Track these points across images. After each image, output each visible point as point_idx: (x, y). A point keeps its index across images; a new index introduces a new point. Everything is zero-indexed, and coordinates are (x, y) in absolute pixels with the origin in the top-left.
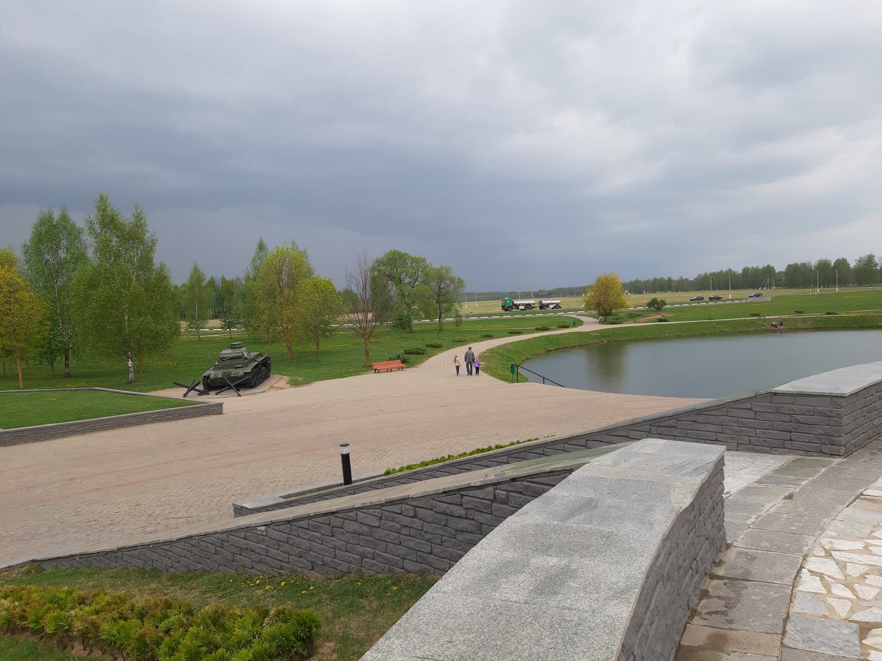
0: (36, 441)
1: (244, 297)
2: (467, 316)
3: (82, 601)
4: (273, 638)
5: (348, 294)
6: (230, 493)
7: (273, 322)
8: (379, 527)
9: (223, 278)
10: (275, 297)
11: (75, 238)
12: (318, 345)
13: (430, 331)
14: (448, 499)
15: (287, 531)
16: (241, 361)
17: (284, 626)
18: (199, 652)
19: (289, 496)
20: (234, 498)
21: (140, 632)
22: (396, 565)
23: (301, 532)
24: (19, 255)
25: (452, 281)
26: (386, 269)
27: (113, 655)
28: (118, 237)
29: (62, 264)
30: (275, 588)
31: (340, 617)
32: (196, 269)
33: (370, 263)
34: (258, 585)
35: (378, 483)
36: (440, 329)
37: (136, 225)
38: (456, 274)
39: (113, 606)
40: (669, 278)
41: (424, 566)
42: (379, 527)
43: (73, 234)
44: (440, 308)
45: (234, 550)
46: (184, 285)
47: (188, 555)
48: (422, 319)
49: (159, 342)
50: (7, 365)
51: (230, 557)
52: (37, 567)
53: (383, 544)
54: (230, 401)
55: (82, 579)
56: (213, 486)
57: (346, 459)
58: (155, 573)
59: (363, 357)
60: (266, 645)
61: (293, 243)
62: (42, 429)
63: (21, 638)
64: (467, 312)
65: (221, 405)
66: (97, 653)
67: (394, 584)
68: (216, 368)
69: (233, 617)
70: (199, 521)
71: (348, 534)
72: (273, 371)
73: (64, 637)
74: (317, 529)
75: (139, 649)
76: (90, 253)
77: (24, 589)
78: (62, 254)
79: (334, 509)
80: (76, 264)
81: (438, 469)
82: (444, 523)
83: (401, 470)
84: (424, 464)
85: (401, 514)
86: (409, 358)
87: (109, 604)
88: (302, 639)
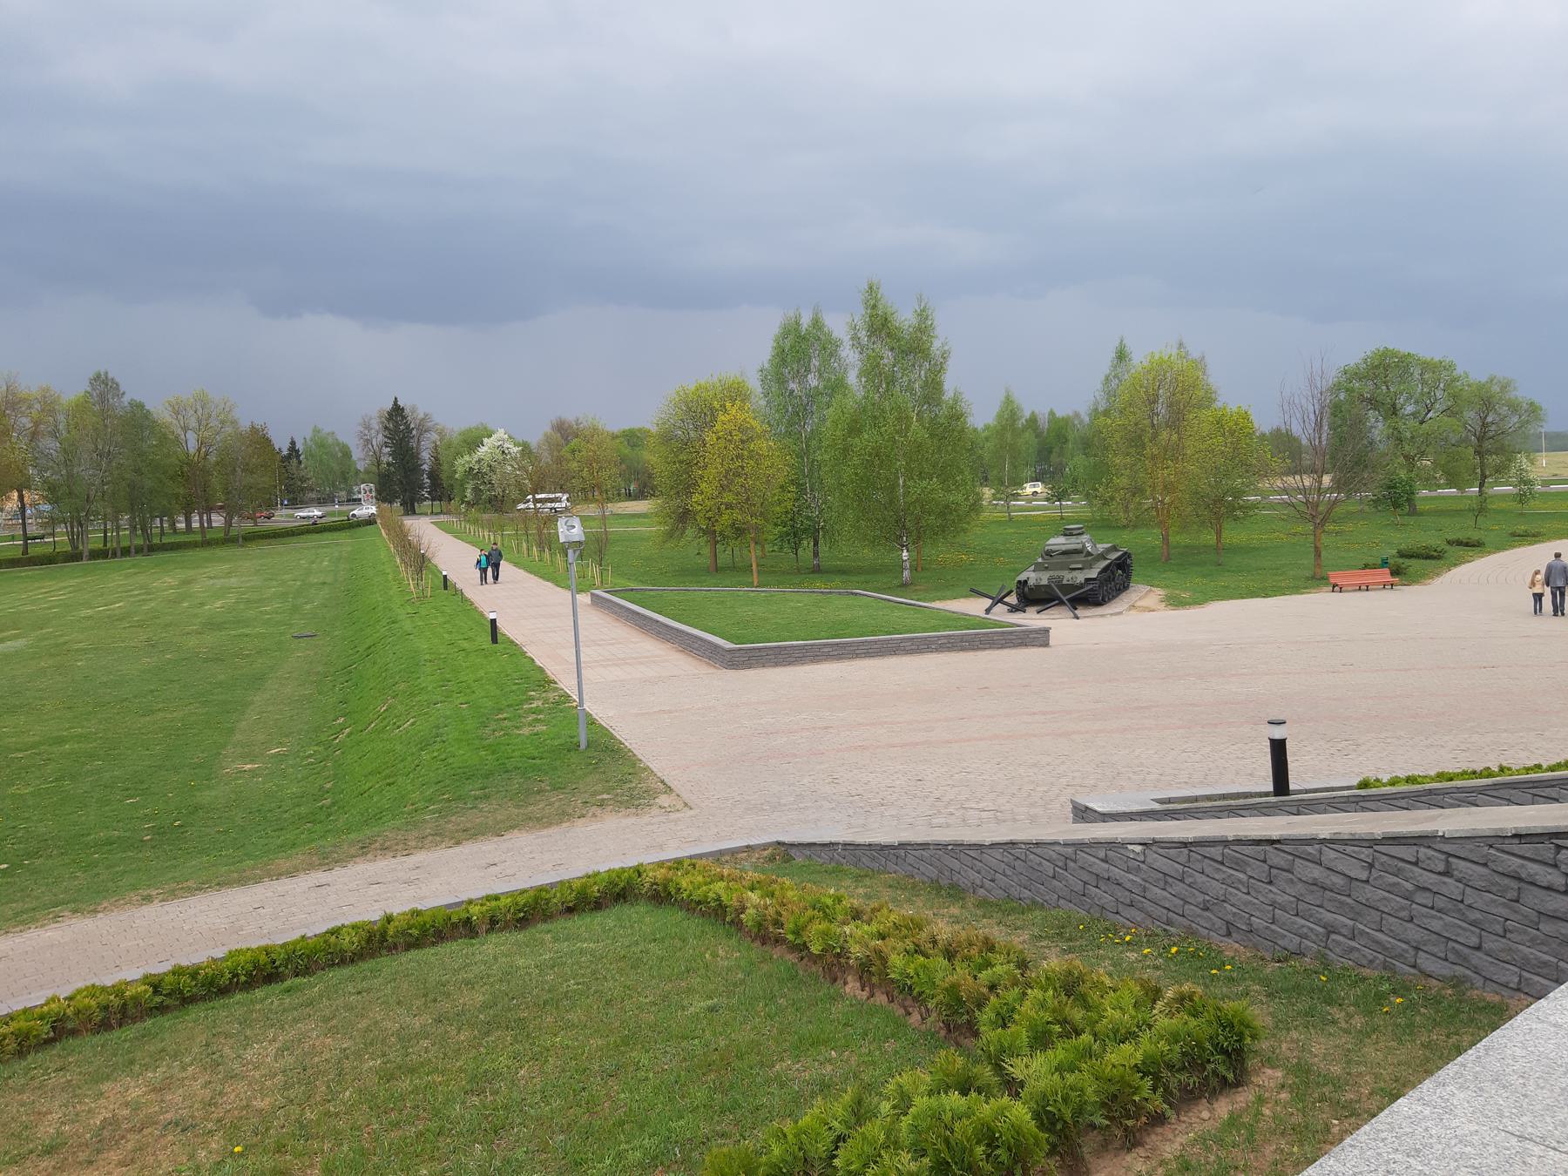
0: (776, 665)
1: (1086, 445)
2: (1546, 483)
3: (856, 915)
4: (1174, 1038)
5: (1283, 442)
6: (1064, 781)
7: (1137, 491)
8: (1367, 881)
9: (1052, 413)
10: (1144, 446)
11: (831, 355)
12: (1219, 534)
13: (1459, 512)
14: (1526, 849)
15: (1182, 859)
16: (1081, 558)
17: (1193, 1022)
18: (1050, 1032)
19: (1169, 801)
20: (1070, 790)
21: (950, 979)
22: (1399, 957)
23: (1208, 866)
24: (754, 385)
25: (1514, 408)
26: (1367, 389)
27: (905, 1008)
28: (892, 349)
29: (813, 395)
30: (1160, 955)
31: (1288, 1030)
32: (1008, 401)
33: (1332, 376)
34: (1128, 943)
35: (1347, 800)
36: (1481, 509)
37: (919, 329)
38: (1523, 392)
39: (905, 931)
40: (104, 386)
41: (1459, 970)
42: (1367, 881)
43: (829, 348)
44: (1482, 465)
45: (1086, 877)
46: (987, 428)
47: (1008, 872)
48: (1439, 487)
49: (947, 521)
50: (736, 549)
51: (1079, 887)
52: (784, 852)
53: (1376, 915)
54: (1059, 623)
55: (848, 882)
56: (1035, 765)
57: (1279, 749)
58: (955, 892)
59: (1309, 560)
60: (1163, 1046)
61: (1181, 345)
62: (785, 648)
63: (777, 952)
64: (1546, 475)
65: (1047, 631)
66: (881, 999)
67: (1394, 992)
68: (1039, 568)
69: (1097, 985)
70: (1015, 820)
71: (1300, 885)
72: (1134, 578)
73: (833, 963)
74: (1239, 865)
75: (949, 1006)
76: (852, 378)
77: (775, 882)
78: (813, 381)
79: (1275, 835)
80: (831, 396)
81: (1481, 791)
82: (1512, 894)
83: (1393, 783)
84: (1441, 776)
85: (1416, 864)
86: (1407, 566)
87: (896, 927)
88: (1224, 1052)
